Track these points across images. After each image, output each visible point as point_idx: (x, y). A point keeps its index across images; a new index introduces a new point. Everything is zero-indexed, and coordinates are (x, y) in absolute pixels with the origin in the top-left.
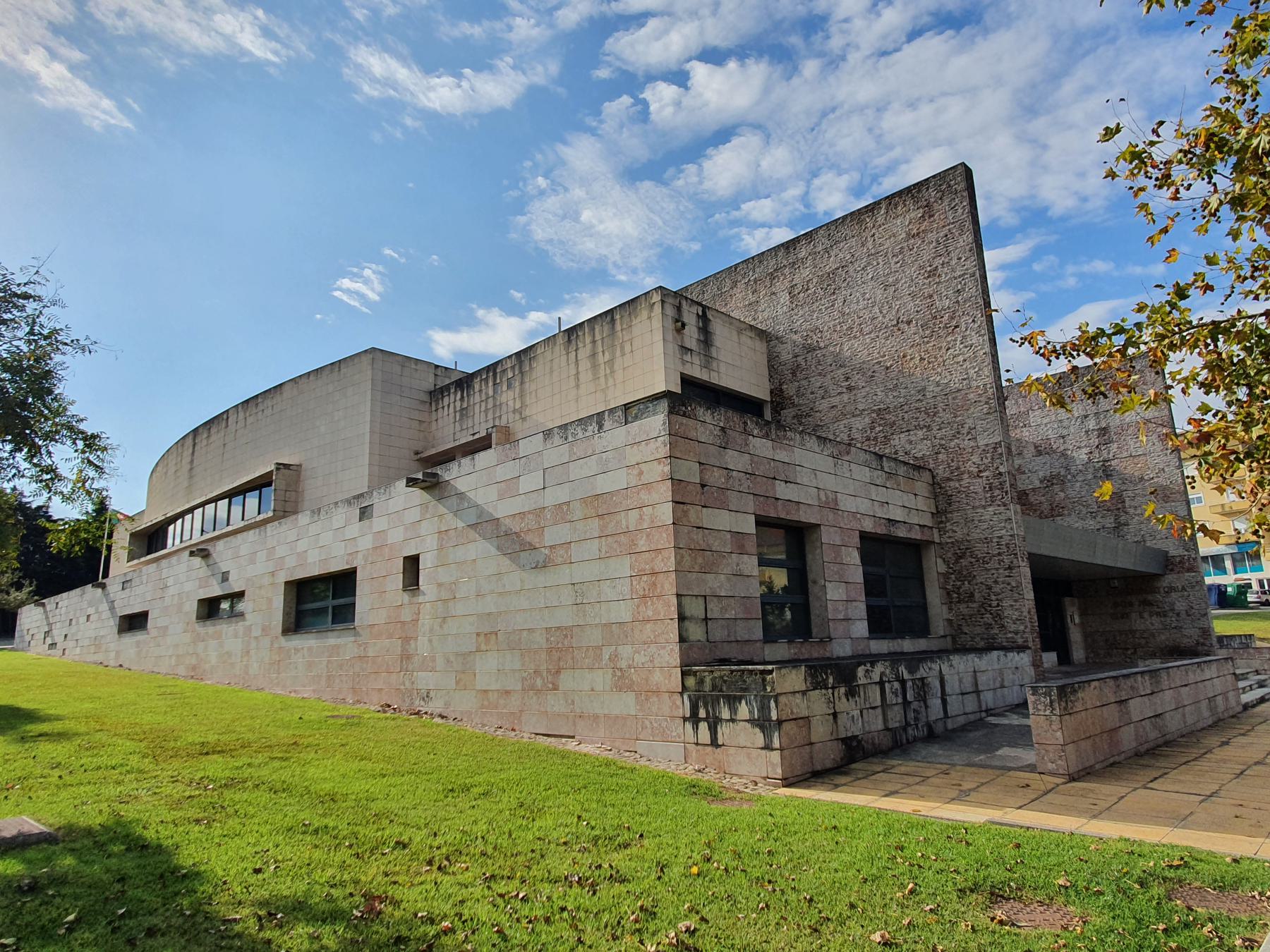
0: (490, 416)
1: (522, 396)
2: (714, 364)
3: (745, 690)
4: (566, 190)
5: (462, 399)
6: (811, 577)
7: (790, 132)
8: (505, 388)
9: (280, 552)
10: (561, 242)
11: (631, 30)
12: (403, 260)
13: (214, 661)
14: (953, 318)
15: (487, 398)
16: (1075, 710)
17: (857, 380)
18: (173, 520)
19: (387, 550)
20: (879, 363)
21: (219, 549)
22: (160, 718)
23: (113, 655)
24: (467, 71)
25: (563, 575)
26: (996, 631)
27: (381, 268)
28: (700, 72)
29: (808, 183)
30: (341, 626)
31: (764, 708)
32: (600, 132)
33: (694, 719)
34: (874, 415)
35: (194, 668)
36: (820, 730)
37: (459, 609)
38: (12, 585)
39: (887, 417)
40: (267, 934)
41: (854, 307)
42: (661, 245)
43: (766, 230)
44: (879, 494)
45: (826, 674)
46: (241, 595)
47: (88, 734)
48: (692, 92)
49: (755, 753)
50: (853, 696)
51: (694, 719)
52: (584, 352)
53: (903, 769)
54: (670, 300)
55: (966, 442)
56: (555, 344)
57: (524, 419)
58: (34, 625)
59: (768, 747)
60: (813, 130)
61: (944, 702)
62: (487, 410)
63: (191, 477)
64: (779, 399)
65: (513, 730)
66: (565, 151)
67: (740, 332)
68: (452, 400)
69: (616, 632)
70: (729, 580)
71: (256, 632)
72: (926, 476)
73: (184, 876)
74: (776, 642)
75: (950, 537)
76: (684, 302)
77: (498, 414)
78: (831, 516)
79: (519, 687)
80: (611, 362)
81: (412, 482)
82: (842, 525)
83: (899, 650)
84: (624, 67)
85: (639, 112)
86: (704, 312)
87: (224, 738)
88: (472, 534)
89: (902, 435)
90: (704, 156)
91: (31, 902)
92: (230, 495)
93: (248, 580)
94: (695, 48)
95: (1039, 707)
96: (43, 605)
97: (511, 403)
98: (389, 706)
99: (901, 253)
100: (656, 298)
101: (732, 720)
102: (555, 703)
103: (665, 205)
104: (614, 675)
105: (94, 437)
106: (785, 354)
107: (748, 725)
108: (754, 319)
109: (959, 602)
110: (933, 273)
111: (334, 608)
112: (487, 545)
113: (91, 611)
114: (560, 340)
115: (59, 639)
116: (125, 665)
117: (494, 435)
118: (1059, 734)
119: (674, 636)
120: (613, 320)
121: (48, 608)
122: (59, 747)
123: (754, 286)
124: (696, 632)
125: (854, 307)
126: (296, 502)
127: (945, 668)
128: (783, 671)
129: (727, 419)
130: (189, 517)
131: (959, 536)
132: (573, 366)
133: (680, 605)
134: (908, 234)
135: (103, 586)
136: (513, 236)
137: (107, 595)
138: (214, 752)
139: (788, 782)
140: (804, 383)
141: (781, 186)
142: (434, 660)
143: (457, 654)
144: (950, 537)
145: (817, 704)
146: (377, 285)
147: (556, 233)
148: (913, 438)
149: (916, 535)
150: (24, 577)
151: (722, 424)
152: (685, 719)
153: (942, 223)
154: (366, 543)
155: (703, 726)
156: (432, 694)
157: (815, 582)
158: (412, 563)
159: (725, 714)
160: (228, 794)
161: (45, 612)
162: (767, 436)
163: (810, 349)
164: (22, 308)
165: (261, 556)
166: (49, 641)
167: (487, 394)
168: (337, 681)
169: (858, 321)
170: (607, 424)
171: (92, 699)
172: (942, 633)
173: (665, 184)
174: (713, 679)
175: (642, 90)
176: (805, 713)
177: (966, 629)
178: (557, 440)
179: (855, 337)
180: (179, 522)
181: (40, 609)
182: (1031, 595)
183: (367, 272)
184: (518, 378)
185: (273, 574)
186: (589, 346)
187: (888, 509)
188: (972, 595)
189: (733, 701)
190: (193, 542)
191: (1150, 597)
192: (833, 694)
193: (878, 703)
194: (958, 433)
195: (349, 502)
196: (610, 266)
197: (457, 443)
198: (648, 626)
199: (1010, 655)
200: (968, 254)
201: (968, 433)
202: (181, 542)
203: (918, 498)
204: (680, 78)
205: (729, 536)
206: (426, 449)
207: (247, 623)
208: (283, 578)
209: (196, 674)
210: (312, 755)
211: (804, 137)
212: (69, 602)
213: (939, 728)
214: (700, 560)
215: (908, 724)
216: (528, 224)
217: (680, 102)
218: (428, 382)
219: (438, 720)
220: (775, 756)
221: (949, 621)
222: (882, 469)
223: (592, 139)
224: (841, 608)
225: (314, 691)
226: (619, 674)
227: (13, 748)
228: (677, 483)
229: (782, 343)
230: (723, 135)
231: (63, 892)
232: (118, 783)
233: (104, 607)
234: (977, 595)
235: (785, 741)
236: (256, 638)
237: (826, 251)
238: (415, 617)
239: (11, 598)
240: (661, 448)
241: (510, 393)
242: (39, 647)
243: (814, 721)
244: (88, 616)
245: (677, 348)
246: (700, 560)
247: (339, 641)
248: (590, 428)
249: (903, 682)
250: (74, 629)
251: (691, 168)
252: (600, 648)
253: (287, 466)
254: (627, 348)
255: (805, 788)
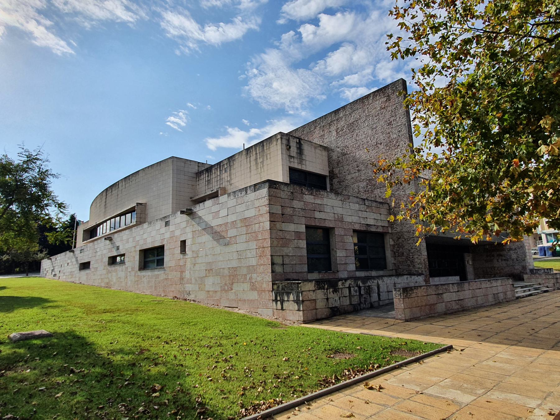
0: (219, 183)
1: (230, 175)
2: (304, 162)
3: (292, 290)
4: (266, 74)
5: (208, 176)
6: (331, 248)
7: (366, 44)
8: (224, 172)
9: (138, 238)
10: (265, 97)
11: (294, 1)
12: (195, 108)
13: (114, 280)
14: (397, 142)
15: (217, 176)
16: (411, 296)
17: (362, 167)
18: (99, 225)
19: (174, 238)
20: (370, 160)
21: (116, 237)
22: (91, 301)
23: (77, 279)
24: (222, 24)
25: (233, 248)
26: (411, 268)
27: (186, 112)
28: (324, 18)
29: (375, 66)
30: (159, 267)
31: (298, 296)
32: (280, 48)
33: (276, 300)
34: (368, 181)
35: (107, 283)
36: (321, 304)
37: (199, 260)
38: (38, 251)
39: (373, 182)
40: (109, 357)
41: (361, 137)
42: (308, 97)
43: (356, 88)
44: (365, 214)
45: (324, 284)
46: (124, 255)
47: (64, 306)
48: (321, 28)
49: (295, 312)
50: (336, 292)
51: (276, 300)
52: (253, 158)
53: (351, 318)
54: (285, 137)
55: (402, 193)
56: (242, 154)
57: (231, 185)
58: (48, 267)
59: (299, 310)
60: (377, 42)
61: (379, 295)
62: (217, 181)
63: (105, 208)
64: (332, 175)
65: (218, 305)
66: (265, 57)
67: (315, 148)
68: (204, 176)
69: (251, 269)
70: (293, 250)
71: (129, 269)
72: (386, 206)
73: (89, 344)
74: (313, 272)
75: (395, 231)
76: (291, 138)
77: (221, 183)
78: (340, 224)
79: (220, 290)
80: (262, 162)
81: (182, 212)
82: (345, 227)
83: (370, 275)
84: (291, 18)
85: (298, 38)
86: (299, 141)
87: (113, 308)
88: (204, 232)
89: (378, 190)
90: (328, 56)
91: (44, 350)
92: (120, 215)
93: (126, 249)
94: (322, 8)
95: (397, 295)
96: (51, 259)
97: (226, 178)
98: (176, 297)
99: (378, 115)
100: (279, 137)
101: (288, 301)
102: (231, 295)
103: (310, 79)
104: (251, 285)
105: (62, 203)
106: (334, 156)
107: (293, 302)
108: (323, 142)
109: (398, 256)
110: (390, 124)
111: (157, 260)
112: (209, 237)
113: (69, 261)
114: (244, 153)
115: (57, 273)
116: (82, 283)
117: (219, 191)
118: (403, 305)
119: (270, 270)
120: (263, 145)
121: (53, 260)
122: (55, 310)
123: (323, 128)
124: (279, 269)
125: (361, 137)
126: (145, 218)
127: (380, 282)
128: (305, 283)
129: (294, 189)
130: (105, 224)
131: (399, 230)
132: (249, 163)
133: (272, 259)
134: (381, 108)
135: (73, 252)
136: (243, 95)
137: (75, 255)
138: (108, 312)
139: (305, 322)
140: (342, 168)
141: (363, 68)
142: (191, 280)
143: (199, 277)
144: (395, 231)
145: (320, 295)
146: (185, 120)
147: (262, 93)
148: (382, 191)
149: (380, 230)
150: (43, 248)
151: (291, 191)
152: (273, 301)
153: (393, 103)
154: (167, 235)
155: (279, 303)
156: (191, 293)
157: (333, 249)
158: (183, 243)
159: (286, 299)
160: (108, 324)
161: (52, 262)
162: (311, 194)
163: (344, 154)
164: (35, 163)
165: (131, 240)
166: (53, 273)
167: (217, 174)
168: (158, 288)
169: (362, 143)
170: (249, 192)
171: (68, 295)
172: (391, 269)
173: (310, 69)
174: (282, 286)
175: (299, 27)
176: (314, 298)
177: (401, 267)
178: (232, 197)
179: (361, 150)
180: (101, 226)
181: (50, 261)
182: (426, 253)
183: (181, 114)
184: (229, 168)
185: (135, 247)
186: (255, 155)
187: (367, 220)
188: (403, 253)
189: (288, 294)
190: (107, 234)
191: (502, 253)
192: (327, 291)
193: (348, 294)
194: (399, 189)
195: (161, 219)
196: (287, 107)
197: (206, 194)
198: (262, 267)
199: (413, 277)
200: (403, 116)
201: (402, 189)
202: (103, 234)
203: (382, 215)
204: (315, 21)
205: (293, 233)
206: (195, 196)
207: (126, 266)
208: (138, 248)
209: (108, 286)
210: (141, 313)
211: (373, 46)
212: (60, 258)
213: (376, 304)
214: (281, 242)
215: (361, 303)
216: (249, 90)
217: (316, 32)
218: (195, 169)
219: (192, 302)
220: (301, 313)
221: (394, 263)
222: (365, 204)
223: (277, 51)
224: (343, 259)
225: (150, 292)
226: (252, 284)
227: (40, 311)
228: (271, 214)
229: (333, 152)
230: (335, 46)
231: (53, 348)
232: (74, 321)
233: (74, 260)
234: (405, 253)
235: (305, 308)
236: (130, 272)
237: (350, 114)
238: (185, 264)
239: (38, 256)
240: (265, 201)
241: (226, 174)
242: (50, 276)
243: (318, 301)
244: (68, 263)
245: (287, 156)
246: (281, 242)
247: (159, 273)
248: (243, 193)
249: (360, 288)
250: (63, 268)
251: (322, 62)
252: (246, 275)
253: (141, 204)
254: (269, 157)
255: (319, 325)
